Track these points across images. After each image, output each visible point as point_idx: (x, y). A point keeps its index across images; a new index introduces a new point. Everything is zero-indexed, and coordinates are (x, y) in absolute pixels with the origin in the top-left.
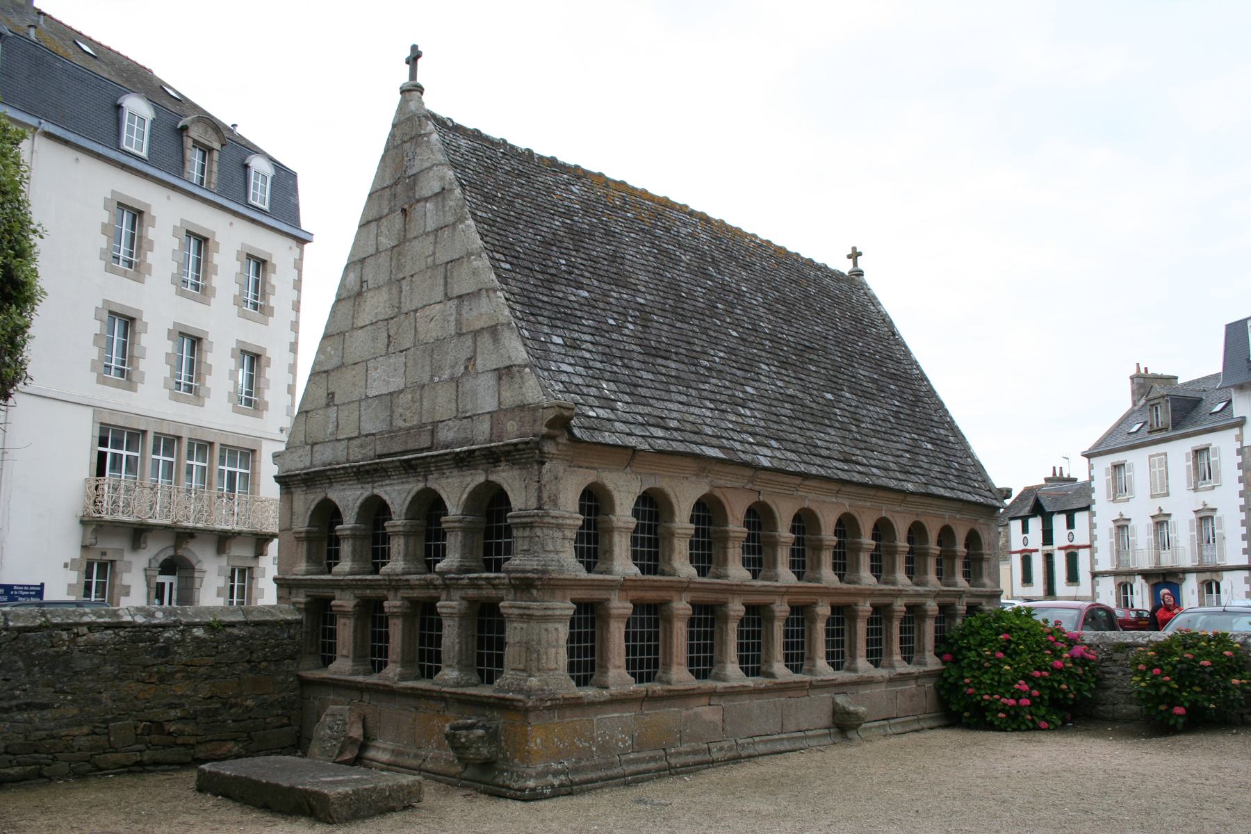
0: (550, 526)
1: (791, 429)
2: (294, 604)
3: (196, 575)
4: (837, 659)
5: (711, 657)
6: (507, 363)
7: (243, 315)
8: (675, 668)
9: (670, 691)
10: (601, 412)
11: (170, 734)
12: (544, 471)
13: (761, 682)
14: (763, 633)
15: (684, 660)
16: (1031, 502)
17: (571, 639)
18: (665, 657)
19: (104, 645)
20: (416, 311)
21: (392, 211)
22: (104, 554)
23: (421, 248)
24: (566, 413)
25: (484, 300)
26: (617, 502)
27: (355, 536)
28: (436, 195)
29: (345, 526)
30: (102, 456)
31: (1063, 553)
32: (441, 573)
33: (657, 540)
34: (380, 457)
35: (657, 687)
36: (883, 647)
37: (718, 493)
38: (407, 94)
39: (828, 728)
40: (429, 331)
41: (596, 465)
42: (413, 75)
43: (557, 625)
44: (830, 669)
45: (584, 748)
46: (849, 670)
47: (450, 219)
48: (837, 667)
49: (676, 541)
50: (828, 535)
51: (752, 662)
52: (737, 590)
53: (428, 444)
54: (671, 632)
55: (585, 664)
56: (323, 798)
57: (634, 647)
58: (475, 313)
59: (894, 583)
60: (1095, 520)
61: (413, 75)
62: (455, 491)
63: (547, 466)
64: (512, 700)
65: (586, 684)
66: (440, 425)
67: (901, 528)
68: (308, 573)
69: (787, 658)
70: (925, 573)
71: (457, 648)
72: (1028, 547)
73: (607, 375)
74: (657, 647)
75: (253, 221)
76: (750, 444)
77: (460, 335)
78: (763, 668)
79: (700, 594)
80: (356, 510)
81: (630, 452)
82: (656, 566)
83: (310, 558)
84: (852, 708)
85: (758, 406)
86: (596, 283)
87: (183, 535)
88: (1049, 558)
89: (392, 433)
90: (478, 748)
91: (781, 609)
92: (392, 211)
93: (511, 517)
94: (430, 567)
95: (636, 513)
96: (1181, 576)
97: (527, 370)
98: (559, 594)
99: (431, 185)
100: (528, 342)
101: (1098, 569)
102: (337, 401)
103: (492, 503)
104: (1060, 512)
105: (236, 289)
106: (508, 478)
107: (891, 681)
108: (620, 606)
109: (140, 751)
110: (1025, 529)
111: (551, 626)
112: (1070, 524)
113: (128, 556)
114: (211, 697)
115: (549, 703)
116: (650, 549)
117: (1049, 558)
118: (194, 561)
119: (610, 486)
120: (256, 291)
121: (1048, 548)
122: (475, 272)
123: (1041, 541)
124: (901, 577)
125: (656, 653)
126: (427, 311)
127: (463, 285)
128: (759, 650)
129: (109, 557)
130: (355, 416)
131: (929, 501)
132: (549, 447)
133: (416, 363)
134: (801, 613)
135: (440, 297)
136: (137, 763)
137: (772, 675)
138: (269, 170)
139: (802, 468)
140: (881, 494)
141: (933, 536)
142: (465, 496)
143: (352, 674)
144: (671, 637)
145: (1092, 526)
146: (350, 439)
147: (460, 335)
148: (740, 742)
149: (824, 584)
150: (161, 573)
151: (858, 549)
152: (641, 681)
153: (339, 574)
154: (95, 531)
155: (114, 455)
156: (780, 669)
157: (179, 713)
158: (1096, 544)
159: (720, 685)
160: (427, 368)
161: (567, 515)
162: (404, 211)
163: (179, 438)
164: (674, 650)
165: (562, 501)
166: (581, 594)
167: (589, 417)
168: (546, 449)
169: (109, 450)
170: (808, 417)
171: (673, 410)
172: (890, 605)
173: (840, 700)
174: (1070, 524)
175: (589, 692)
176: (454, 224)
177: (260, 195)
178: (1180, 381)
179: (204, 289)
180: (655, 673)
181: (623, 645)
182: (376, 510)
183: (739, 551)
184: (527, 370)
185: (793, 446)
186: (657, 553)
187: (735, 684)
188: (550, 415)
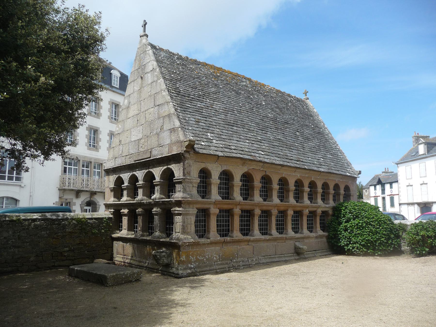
0: (188, 182)
1: (278, 150)
2: (110, 212)
3: (97, 206)
4: (296, 230)
5: (249, 228)
6: (173, 127)
7: (111, 122)
8: (235, 232)
9: (233, 240)
10: (207, 144)
11: (65, 256)
12: (185, 163)
13: (267, 237)
14: (268, 220)
15: (238, 229)
16: (377, 180)
17: (196, 221)
18: (231, 228)
19: (41, 226)
20: (146, 111)
21: (138, 78)
22: (66, 200)
23: (147, 89)
24: (192, 143)
25: (166, 106)
26: (213, 174)
27: (127, 188)
28: (151, 71)
29: (125, 185)
30: (65, 168)
31: (389, 197)
32: (153, 200)
33: (228, 188)
34: (135, 161)
35: (228, 239)
36: (314, 226)
37: (250, 172)
38: (142, 37)
39: (293, 253)
40: (150, 117)
41: (204, 161)
42: (145, 31)
43: (191, 217)
44: (293, 233)
45: (201, 260)
46: (301, 233)
47: (156, 79)
48: (296, 232)
49: (235, 188)
50: (292, 187)
51: (264, 230)
52: (258, 205)
53: (149, 156)
54: (234, 219)
55: (202, 230)
56: (105, 277)
57: (220, 225)
58: (163, 110)
59: (317, 203)
60: (400, 185)
61: (145, 31)
62: (157, 172)
63: (187, 162)
64: (175, 243)
65: (202, 237)
66: (153, 149)
67: (319, 185)
68: (114, 201)
69: (277, 229)
70: (329, 199)
71: (159, 225)
72: (377, 195)
73: (210, 131)
74: (229, 225)
75: (114, 91)
76: (262, 154)
77: (159, 118)
78: (268, 232)
79: (251, 207)
80: (128, 179)
81: (217, 157)
82: (228, 197)
83: (115, 197)
84: (301, 247)
85: (266, 142)
86: (208, 101)
87: (93, 193)
88: (384, 198)
89: (139, 153)
90: (163, 260)
91: (275, 212)
92: (138, 78)
93: (175, 180)
94: (169, 197)
95: (220, 178)
96: (431, 204)
97: (180, 129)
98: (191, 206)
99: (149, 68)
100: (182, 120)
101: (401, 202)
102: (122, 143)
103: (168, 175)
104: (387, 183)
105: (108, 114)
106: (174, 167)
107: (316, 237)
108: (214, 211)
109: (54, 262)
110: (375, 189)
111: (188, 217)
112: (391, 187)
113: (75, 200)
114: (79, 244)
115: (187, 244)
116: (226, 192)
117: (384, 198)
118: (96, 202)
119: (210, 168)
120: (116, 114)
121: (383, 195)
122: (163, 96)
123: (381, 193)
124: (319, 201)
125: (229, 227)
126: (149, 111)
127: (160, 101)
128: (267, 226)
129: (68, 201)
130: (127, 148)
131: (330, 175)
132: (187, 155)
133: (146, 129)
134: (283, 214)
135: (153, 106)
136: (53, 266)
137: (271, 235)
138: (119, 75)
139: (281, 163)
140: (311, 172)
141: (331, 187)
142: (161, 173)
143: (127, 235)
144: (233, 221)
145: (399, 188)
146: (126, 156)
147: (159, 118)
148: (260, 258)
149: (290, 203)
150: (87, 206)
151: (303, 192)
152: (223, 236)
153: (122, 201)
154: (63, 192)
155: (69, 168)
156: (274, 232)
157: (67, 249)
158: (400, 194)
159: (252, 238)
160: (149, 130)
161: (194, 178)
162: (142, 78)
163: (91, 162)
164: (235, 225)
165: (192, 174)
166: (199, 206)
167: (202, 145)
168: (186, 156)
169: (68, 166)
170: (285, 146)
171: (233, 144)
172: (316, 211)
173: (297, 244)
174: (391, 187)
175: (203, 240)
176: (157, 81)
177: (116, 83)
178: (430, 137)
179: (98, 114)
180: (228, 234)
181: (216, 224)
182: (134, 179)
183: (258, 192)
184: (180, 129)
185: (279, 156)
186: (228, 192)
187: (257, 238)
188: (187, 143)
